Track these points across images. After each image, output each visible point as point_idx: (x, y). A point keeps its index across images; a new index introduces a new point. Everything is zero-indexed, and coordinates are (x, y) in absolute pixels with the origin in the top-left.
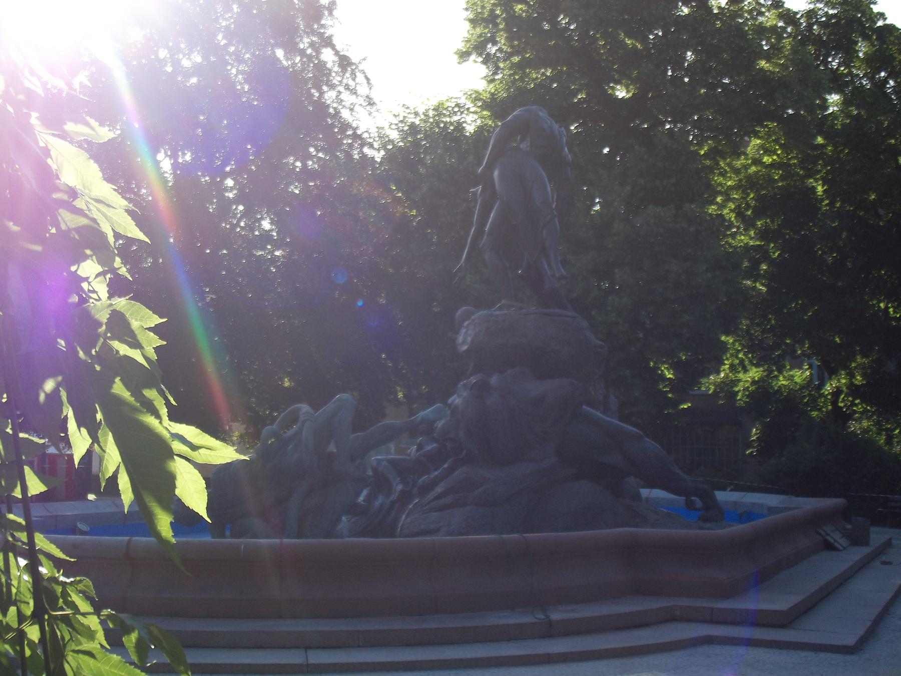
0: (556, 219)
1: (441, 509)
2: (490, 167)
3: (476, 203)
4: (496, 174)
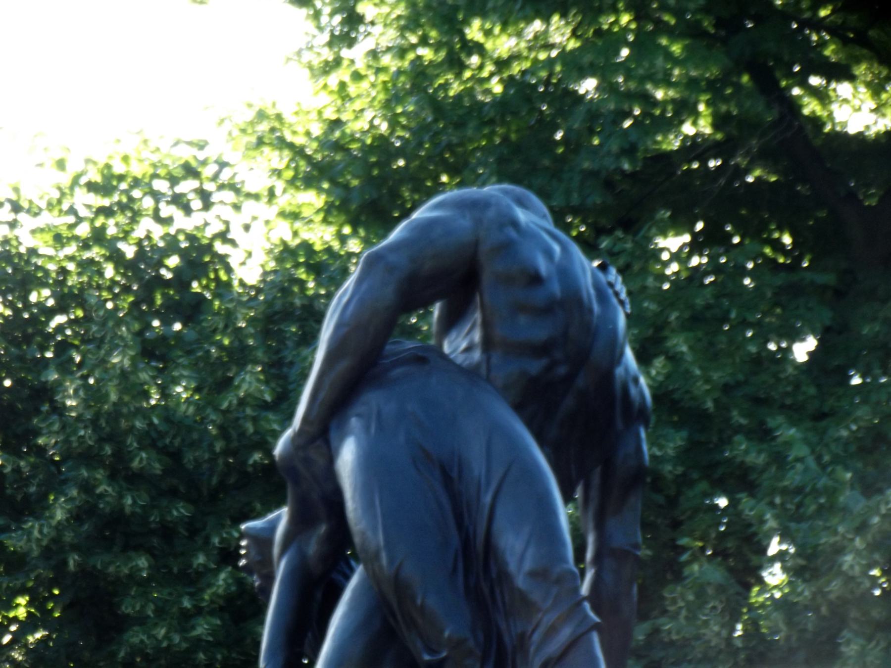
0: (595, 638)
2: (322, 433)
3: (269, 579)
4: (348, 456)
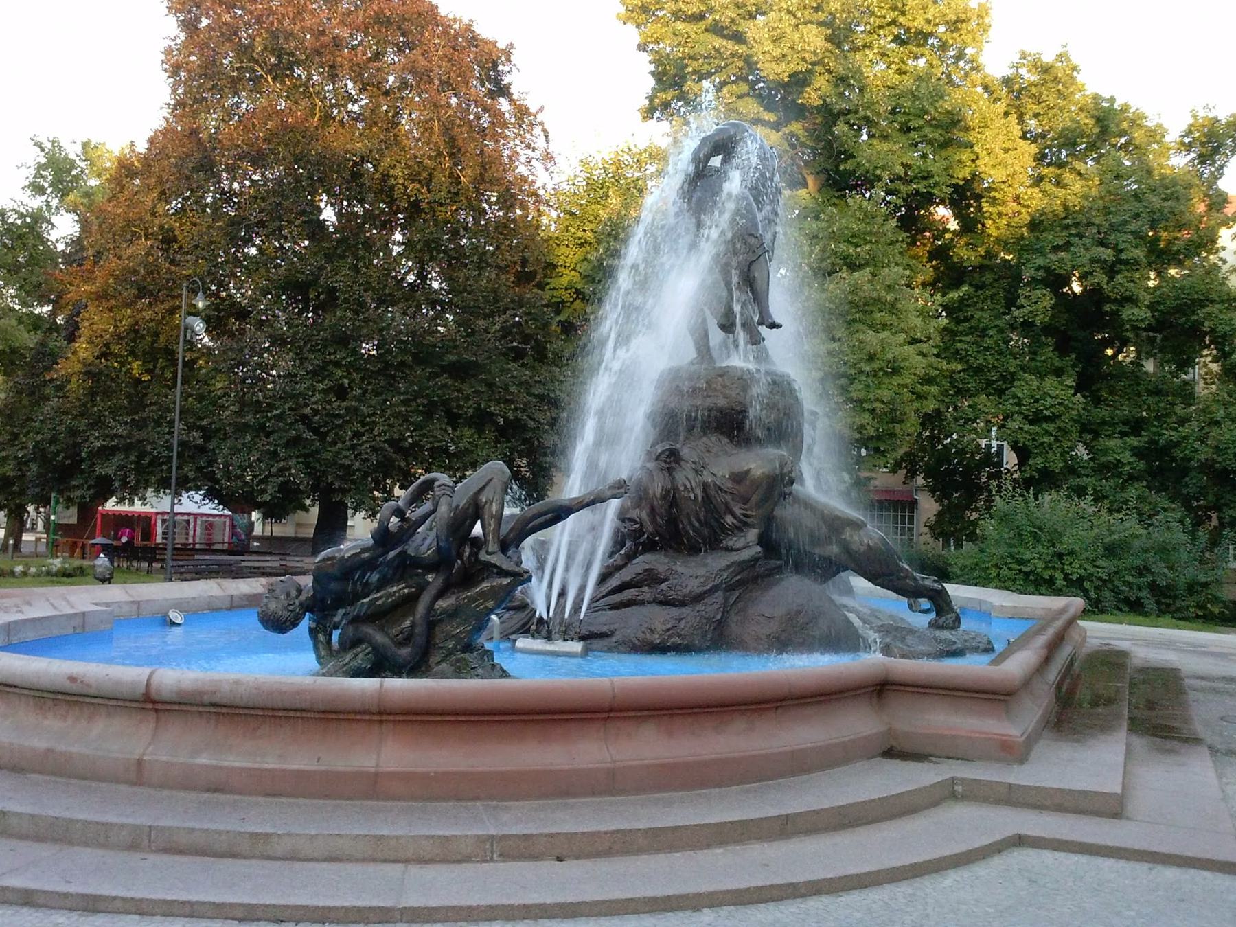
1: (615, 607)
